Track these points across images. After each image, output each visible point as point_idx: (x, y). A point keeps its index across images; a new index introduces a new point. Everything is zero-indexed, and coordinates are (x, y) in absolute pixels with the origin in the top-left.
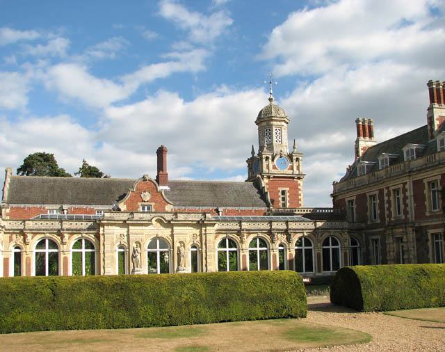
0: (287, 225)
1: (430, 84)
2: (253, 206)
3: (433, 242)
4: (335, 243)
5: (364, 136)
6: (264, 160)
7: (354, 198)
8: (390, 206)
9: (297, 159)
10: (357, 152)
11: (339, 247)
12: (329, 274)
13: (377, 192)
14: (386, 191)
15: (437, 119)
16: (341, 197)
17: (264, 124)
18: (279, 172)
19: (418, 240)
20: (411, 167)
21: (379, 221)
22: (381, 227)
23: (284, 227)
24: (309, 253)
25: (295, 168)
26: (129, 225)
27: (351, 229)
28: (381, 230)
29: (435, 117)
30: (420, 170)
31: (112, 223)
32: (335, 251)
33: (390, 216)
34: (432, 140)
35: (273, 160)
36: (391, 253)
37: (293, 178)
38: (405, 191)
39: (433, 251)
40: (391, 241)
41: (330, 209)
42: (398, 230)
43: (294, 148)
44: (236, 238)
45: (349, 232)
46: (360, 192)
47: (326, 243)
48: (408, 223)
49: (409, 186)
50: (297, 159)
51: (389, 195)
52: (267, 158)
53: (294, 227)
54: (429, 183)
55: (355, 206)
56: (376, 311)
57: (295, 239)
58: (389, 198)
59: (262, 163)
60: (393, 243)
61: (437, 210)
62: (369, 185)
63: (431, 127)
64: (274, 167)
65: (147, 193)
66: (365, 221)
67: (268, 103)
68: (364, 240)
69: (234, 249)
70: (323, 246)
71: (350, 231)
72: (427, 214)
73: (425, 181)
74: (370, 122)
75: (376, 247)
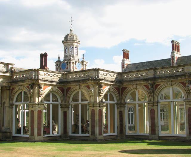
5: (126, 58)
6: (72, 64)
29: (175, 57)
35: (75, 64)
43: (83, 58)
56: (110, 88)
63: (173, 61)
72: (116, 74)
74: (128, 52)
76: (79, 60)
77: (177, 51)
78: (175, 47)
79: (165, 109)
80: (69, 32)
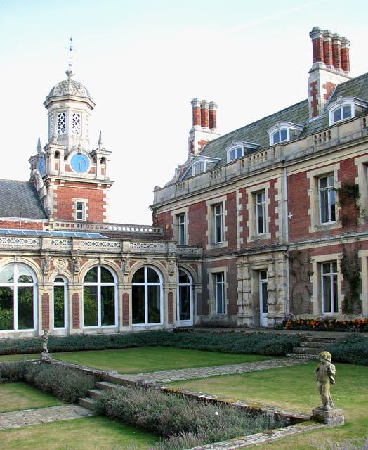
0: (71, 244)
1: (314, 33)
2: (20, 216)
3: (319, 276)
6: (52, 156)
7: (186, 210)
8: (246, 219)
9: (103, 159)
10: (192, 147)
12: (144, 329)
13: (224, 199)
14: (239, 196)
15: (324, 86)
16: (164, 210)
17: (56, 105)
18: (74, 175)
19: (293, 273)
20: (286, 154)
21: (225, 244)
22: (228, 254)
23: (66, 248)
24: (108, 294)
27: (181, 255)
28: (229, 258)
30: (301, 160)
32: (154, 292)
33: (245, 234)
34: (315, 119)
35: (66, 158)
36: (246, 295)
37: (96, 185)
38: (273, 192)
39: (320, 291)
40: (246, 275)
41: (148, 227)
42: (257, 258)
45: (177, 261)
46: (196, 200)
47: (139, 276)
48: (278, 246)
49: (281, 185)
50: (103, 159)
51: (244, 201)
52: (57, 154)
53: (83, 249)
54: (316, 178)
55: (186, 222)
57: (84, 270)
58: (244, 207)
59: (49, 162)
60: (249, 279)
61: (330, 222)
62: (211, 189)
64: (67, 168)
66: (201, 245)
67: (65, 78)
68: (200, 274)
70: (133, 281)
71: (180, 258)
72: (312, 230)
73: (310, 176)
74: (212, 105)
75: (219, 286)
76: (79, 146)
77: (336, 65)
78: (328, 50)
79: (270, 268)
80: (65, 78)
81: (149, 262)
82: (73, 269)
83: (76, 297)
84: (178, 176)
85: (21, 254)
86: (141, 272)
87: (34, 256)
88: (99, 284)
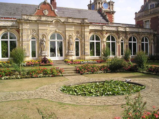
4: (146, 40)
7: (150, 19)
9: (112, 5)
11: (148, 42)
25: (111, 8)
26: (38, 23)
31: (28, 22)
32: (147, 44)
44: (98, 34)
46: (154, 16)
52: (99, 3)
65: (46, 11)
69: (142, 42)
81: (146, 35)
82: (126, 37)
83: (140, 45)
84: (142, 9)
85: (113, 32)
86: (109, 37)
87: (116, 32)
88: (95, 41)
